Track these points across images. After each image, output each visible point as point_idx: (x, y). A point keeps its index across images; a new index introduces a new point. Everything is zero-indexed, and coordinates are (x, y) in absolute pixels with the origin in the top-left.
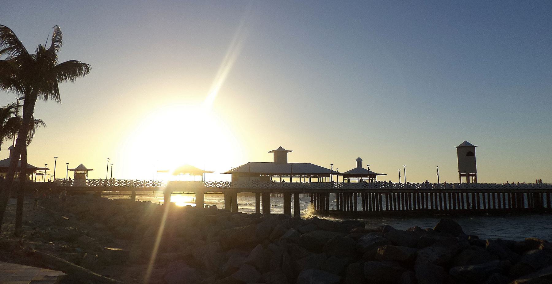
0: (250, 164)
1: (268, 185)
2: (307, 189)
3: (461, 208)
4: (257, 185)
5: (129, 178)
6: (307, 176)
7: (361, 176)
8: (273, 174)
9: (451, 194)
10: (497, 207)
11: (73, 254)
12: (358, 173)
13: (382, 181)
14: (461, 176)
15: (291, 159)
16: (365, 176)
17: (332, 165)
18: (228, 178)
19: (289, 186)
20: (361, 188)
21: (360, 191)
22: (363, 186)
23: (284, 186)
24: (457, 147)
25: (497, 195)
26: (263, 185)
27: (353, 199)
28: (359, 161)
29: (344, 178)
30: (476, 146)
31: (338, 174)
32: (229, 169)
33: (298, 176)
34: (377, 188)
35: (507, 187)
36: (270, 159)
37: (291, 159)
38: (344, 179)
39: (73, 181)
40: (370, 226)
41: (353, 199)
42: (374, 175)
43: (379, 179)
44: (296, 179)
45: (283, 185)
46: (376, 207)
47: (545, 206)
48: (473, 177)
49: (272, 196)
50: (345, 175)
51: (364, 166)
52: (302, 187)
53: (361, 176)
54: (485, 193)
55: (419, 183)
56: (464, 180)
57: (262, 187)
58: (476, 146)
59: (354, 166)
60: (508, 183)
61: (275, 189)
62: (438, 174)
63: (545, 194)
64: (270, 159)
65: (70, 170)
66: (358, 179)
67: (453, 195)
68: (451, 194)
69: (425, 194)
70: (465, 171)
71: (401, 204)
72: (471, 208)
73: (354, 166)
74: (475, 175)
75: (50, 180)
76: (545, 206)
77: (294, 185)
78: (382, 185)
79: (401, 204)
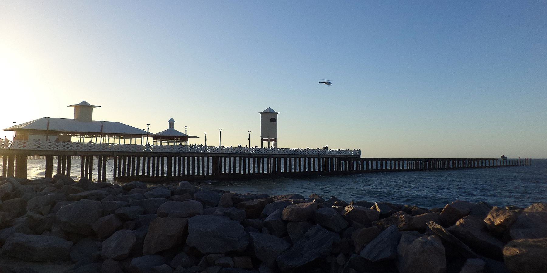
0: (48, 120)
1: (57, 146)
2: (119, 152)
3: (307, 170)
4: (57, 146)
5: (343, 149)
6: (87, 135)
8: (74, 133)
10: (307, 170)
11: (69, 204)
13: (198, 145)
14: (263, 140)
15: (97, 116)
16: (177, 137)
17: (148, 125)
18: (10, 136)
20: (177, 152)
23: (79, 148)
25: (191, 158)
26: (64, 146)
27: (122, 161)
28: (172, 122)
29: (154, 141)
30: (278, 113)
31: (148, 135)
32: (11, 125)
33: (78, 135)
34: (57, 149)
35: (42, 147)
36: (70, 114)
37: (97, 116)
38: (153, 142)
41: (122, 161)
42: (185, 138)
43: (191, 142)
44: (87, 140)
45: (90, 147)
48: (274, 142)
49: (30, 159)
50: (156, 137)
51: (177, 127)
52: (113, 150)
56: (265, 145)
57: (20, 148)
59: (166, 127)
60: (240, 147)
61: (80, 151)
62: (206, 140)
64: (70, 114)
67: (137, 158)
68: (277, 158)
69: (186, 158)
70: (268, 136)
71: (156, 166)
74: (275, 140)
75: (240, 145)
77: (127, 147)
78: (252, 150)
79: (156, 166)
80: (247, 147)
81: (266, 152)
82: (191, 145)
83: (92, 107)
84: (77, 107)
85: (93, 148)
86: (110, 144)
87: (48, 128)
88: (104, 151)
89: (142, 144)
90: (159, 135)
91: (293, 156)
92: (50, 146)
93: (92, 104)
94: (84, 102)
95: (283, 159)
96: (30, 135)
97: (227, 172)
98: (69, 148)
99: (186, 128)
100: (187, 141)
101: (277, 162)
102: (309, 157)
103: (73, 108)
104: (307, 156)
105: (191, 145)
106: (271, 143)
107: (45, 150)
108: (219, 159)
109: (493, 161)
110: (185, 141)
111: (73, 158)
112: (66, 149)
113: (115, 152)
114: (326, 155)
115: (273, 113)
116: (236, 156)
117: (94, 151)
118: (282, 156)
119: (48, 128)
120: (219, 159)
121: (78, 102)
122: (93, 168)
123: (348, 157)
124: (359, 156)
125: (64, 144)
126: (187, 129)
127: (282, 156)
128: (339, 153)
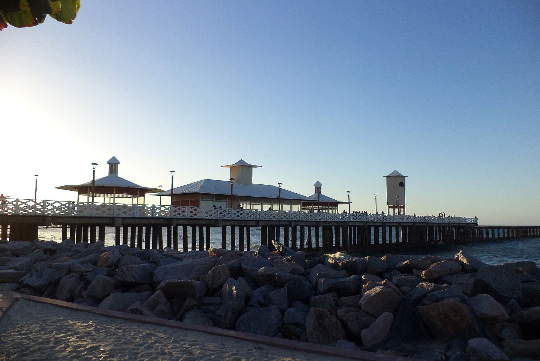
0: (207, 181)
7: (115, 191)
9: (357, 227)
12: (107, 184)
14: (390, 207)
19: (129, 213)
21: (257, 223)
22: (198, 212)
24: (386, 177)
30: (405, 177)
36: (225, 176)
39: (316, 211)
40: (217, 270)
42: (335, 204)
46: (353, 239)
47: (373, 242)
51: (123, 173)
52: (290, 219)
53: (115, 191)
54: (379, 227)
55: (58, 202)
58: (405, 177)
63: (373, 229)
64: (225, 176)
65: (346, 203)
66: (323, 208)
71: (172, 242)
72: (388, 242)
73: (103, 172)
74: (403, 207)
76: (373, 242)
80: (383, 213)
81: (238, 216)
82: (454, 216)
83: (250, 167)
84: (233, 168)
85: (122, 213)
86: (139, 206)
87: (319, 200)
88: (175, 217)
89: (252, 209)
90: (197, 190)
91: (307, 224)
92: (191, 212)
93: (249, 163)
94: (241, 161)
95: (387, 229)
96: (202, 200)
97: (490, 237)
98: (127, 213)
99: (94, 166)
100: (336, 208)
101: (401, 233)
102: (376, 226)
103: (229, 169)
104: (300, 223)
105: (454, 216)
106: (396, 210)
107: (230, 219)
108: (353, 228)
109: (503, 230)
110: (317, 207)
111: (212, 229)
112: (194, 216)
113: (292, 221)
114: (390, 222)
115: (401, 176)
116: (391, 225)
117: (195, 219)
118: (228, 224)
119: (319, 200)
120: (353, 228)
121: (234, 162)
122: (197, 245)
123: (461, 225)
124: (477, 224)
125: (191, 210)
126: (175, 175)
127: (228, 224)
128: (383, 220)
